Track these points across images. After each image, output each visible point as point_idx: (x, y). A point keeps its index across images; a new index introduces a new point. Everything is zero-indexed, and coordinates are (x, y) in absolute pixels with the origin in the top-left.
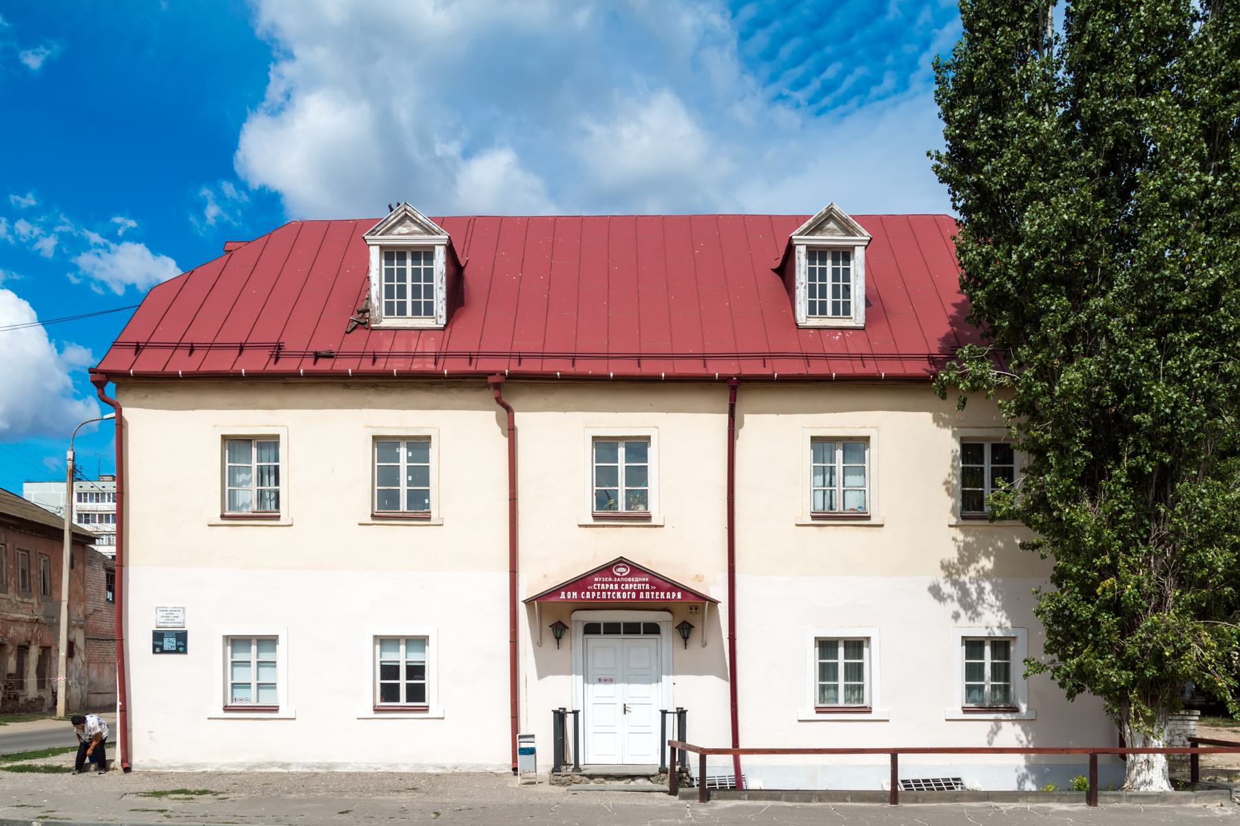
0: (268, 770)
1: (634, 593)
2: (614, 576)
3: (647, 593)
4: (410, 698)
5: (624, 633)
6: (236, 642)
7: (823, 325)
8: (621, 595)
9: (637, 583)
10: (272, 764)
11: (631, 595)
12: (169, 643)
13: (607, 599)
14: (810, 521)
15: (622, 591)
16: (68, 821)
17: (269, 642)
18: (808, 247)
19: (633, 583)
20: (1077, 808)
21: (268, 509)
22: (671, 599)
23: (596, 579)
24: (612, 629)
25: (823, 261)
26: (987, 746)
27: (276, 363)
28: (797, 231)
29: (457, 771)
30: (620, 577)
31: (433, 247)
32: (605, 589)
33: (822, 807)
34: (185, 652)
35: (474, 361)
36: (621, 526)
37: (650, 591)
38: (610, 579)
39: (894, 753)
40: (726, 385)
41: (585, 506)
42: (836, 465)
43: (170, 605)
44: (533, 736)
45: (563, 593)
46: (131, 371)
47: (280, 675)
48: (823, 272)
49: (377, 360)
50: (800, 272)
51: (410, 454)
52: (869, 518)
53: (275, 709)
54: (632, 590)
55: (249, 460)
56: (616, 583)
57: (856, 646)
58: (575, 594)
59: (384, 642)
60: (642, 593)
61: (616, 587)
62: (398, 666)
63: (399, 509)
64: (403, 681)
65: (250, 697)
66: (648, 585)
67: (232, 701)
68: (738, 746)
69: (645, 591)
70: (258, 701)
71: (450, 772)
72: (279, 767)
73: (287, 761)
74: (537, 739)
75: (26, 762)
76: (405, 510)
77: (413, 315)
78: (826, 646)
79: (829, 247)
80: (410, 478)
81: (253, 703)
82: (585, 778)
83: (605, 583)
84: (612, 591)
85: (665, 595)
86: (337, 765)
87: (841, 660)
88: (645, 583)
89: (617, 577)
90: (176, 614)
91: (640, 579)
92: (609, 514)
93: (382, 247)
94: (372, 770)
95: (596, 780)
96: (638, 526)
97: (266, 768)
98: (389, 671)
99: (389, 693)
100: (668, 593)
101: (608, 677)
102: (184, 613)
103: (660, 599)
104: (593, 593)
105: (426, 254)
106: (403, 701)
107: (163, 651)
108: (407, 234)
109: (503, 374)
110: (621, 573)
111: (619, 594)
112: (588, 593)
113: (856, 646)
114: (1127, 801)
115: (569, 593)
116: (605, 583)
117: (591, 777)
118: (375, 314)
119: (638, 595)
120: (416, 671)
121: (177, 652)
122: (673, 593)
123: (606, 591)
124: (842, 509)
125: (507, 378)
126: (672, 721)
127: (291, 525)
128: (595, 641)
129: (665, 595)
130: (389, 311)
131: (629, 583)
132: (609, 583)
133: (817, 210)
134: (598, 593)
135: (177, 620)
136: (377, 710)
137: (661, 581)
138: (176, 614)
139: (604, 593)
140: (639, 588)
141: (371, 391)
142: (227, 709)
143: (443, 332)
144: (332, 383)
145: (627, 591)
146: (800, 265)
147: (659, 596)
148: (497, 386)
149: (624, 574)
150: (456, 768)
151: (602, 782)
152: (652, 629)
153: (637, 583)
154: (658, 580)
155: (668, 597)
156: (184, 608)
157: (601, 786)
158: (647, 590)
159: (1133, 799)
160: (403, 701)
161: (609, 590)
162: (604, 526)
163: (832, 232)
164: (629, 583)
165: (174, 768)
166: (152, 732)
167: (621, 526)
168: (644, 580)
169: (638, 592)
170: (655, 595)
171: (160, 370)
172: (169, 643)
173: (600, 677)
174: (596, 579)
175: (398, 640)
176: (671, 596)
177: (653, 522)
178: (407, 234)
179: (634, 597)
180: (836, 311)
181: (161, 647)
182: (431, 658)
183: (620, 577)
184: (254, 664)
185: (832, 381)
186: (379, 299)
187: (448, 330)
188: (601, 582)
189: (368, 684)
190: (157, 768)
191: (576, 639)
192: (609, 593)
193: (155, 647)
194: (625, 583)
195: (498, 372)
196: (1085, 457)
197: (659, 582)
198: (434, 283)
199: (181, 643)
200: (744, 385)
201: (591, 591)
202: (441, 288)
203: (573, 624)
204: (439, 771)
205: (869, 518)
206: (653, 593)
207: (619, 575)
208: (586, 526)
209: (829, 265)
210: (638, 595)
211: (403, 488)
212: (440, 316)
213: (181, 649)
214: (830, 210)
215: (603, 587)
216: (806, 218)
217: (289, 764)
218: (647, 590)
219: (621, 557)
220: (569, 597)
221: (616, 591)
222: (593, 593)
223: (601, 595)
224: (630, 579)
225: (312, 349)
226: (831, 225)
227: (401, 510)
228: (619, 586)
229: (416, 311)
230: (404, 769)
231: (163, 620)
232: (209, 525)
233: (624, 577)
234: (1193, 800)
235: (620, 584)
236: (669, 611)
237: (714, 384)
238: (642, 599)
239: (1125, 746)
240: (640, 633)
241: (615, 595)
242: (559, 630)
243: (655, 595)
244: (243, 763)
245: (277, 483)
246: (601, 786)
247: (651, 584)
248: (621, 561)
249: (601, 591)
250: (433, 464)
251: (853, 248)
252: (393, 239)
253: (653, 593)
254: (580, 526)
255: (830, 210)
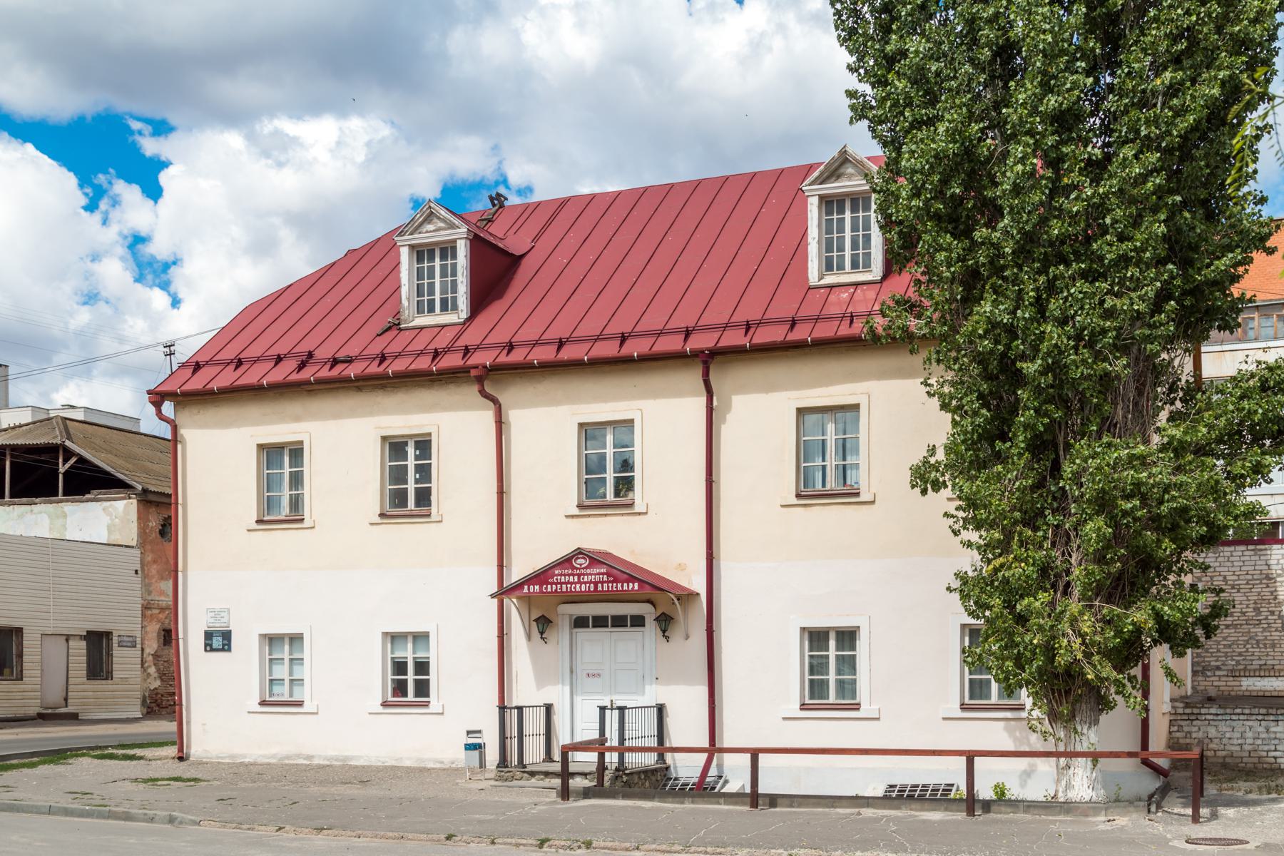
0: (295, 762)
1: (592, 585)
2: (574, 568)
3: (605, 585)
4: (417, 694)
5: (613, 626)
6: (272, 640)
7: (836, 282)
8: (580, 587)
9: (595, 574)
10: (299, 756)
11: (589, 587)
12: (217, 642)
13: (608, 591)
14: (795, 501)
15: (581, 583)
16: (22, 802)
17: (296, 639)
18: (822, 198)
19: (591, 574)
20: (954, 817)
21: (817, 488)
22: (628, 590)
23: (557, 572)
24: (600, 622)
25: (432, 259)
26: (542, 738)
27: (508, 354)
28: (807, 182)
29: (454, 766)
30: (580, 569)
31: (455, 241)
32: (566, 581)
33: (693, 809)
34: (229, 650)
35: (752, 331)
36: (606, 515)
37: (608, 582)
38: (570, 572)
39: (970, 756)
40: (698, 360)
41: (570, 494)
42: (828, 437)
43: (217, 606)
44: (480, 732)
45: (526, 587)
46: (586, 358)
47: (304, 672)
48: (431, 270)
49: (797, 326)
50: (812, 225)
51: (418, 453)
52: (857, 494)
53: (299, 704)
54: (590, 582)
55: (282, 467)
56: (576, 575)
57: (848, 637)
58: (537, 587)
59: (395, 638)
60: (600, 585)
61: (576, 580)
62: (406, 662)
63: (407, 507)
64: (411, 677)
65: (282, 693)
66: (605, 576)
67: (270, 696)
68: (714, 745)
69: (602, 583)
70: (291, 696)
71: (448, 766)
72: (305, 759)
73: (311, 753)
74: (484, 732)
75: (130, 752)
76: (413, 508)
77: (441, 311)
78: (816, 637)
79: (437, 243)
80: (418, 476)
81: (286, 698)
82: (526, 775)
83: (565, 575)
84: (571, 583)
85: (622, 586)
86: (352, 758)
87: (832, 652)
88: (603, 574)
89: (577, 569)
90: (223, 614)
91: (598, 571)
92: (598, 503)
93: (412, 247)
94: (380, 764)
95: (537, 777)
96: (622, 514)
97: (294, 760)
98: (400, 667)
99: (400, 688)
100: (625, 584)
101: (596, 672)
102: (229, 613)
103: (617, 591)
104: (554, 586)
105: (447, 250)
106: (411, 696)
107: (212, 650)
108: (434, 231)
109: (485, 367)
110: (581, 565)
111: (578, 586)
112: (549, 586)
113: (848, 637)
114: (1025, 812)
115: (531, 587)
116: (565, 575)
117: (532, 774)
118: (405, 314)
119: (596, 587)
120: (422, 667)
121: (223, 650)
122: (631, 584)
123: (566, 583)
124: (819, 486)
125: (490, 371)
126: (612, 718)
127: (313, 527)
128: (582, 634)
129: (622, 586)
130: (420, 311)
131: (587, 574)
132: (569, 575)
133: (827, 155)
134: (559, 586)
135: (223, 620)
136: (385, 704)
137: (619, 573)
138: (223, 614)
139: (564, 586)
140: (597, 580)
141: (380, 392)
142: (263, 703)
143: (880, 285)
144: (343, 388)
145: (585, 583)
146: (812, 218)
147: (617, 587)
148: (480, 380)
149: (583, 566)
150: (453, 763)
151: (542, 779)
152: (638, 621)
153: (597, 574)
154: (615, 571)
155: (625, 588)
156: (228, 610)
157: (541, 783)
158: (605, 582)
159: (1032, 809)
160: (411, 696)
161: (569, 582)
162: (589, 516)
163: (850, 177)
164: (587, 574)
165: (222, 758)
166: (204, 724)
167: (606, 515)
168: (602, 571)
169: (596, 584)
170: (612, 587)
171: (404, 368)
172: (217, 642)
173: (588, 671)
174: (557, 572)
175: (283, 638)
176: (628, 587)
177: (637, 509)
178: (434, 231)
179: (592, 589)
180: (444, 308)
181: (211, 645)
182: (433, 655)
183: (580, 569)
184: (287, 661)
185: (265, 388)
186: (409, 299)
187: (885, 284)
188: (561, 575)
189: (376, 680)
190: (208, 758)
191: (562, 634)
192: (569, 586)
193: (206, 645)
194: (584, 575)
195: (480, 364)
196: (983, 415)
197: (628, 573)
198: (872, 232)
199: (226, 642)
200: (718, 358)
201: (552, 584)
202: (462, 282)
203: (560, 617)
204: (438, 766)
205: (857, 494)
206: (610, 585)
207: (578, 566)
208: (573, 516)
209: (438, 263)
210: (596, 587)
211: (411, 487)
212: (462, 311)
213: (226, 647)
214: (843, 152)
215: (563, 580)
216: (820, 164)
217: (313, 757)
218: (605, 582)
219: (579, 548)
220: (531, 591)
221: (576, 583)
222: (554, 586)
223: (561, 588)
224: (588, 571)
225: (740, 317)
226: (850, 170)
227: (409, 508)
228: (579, 579)
229: (444, 308)
230: (408, 763)
231: (212, 620)
232: (249, 530)
233: (583, 569)
234: (1103, 812)
235: (579, 575)
236: (654, 606)
237: (807, 350)
238: (600, 591)
239: (1147, 750)
240: (607, 626)
241: (575, 588)
242: (543, 624)
243: (612, 587)
244: (275, 755)
245: (824, 460)
246: (541, 783)
247: (608, 574)
248: (579, 552)
249: (561, 583)
250: (306, 469)
251: (455, 241)
252: (418, 239)
253: (610, 585)
254: (567, 516)
255: (843, 152)
